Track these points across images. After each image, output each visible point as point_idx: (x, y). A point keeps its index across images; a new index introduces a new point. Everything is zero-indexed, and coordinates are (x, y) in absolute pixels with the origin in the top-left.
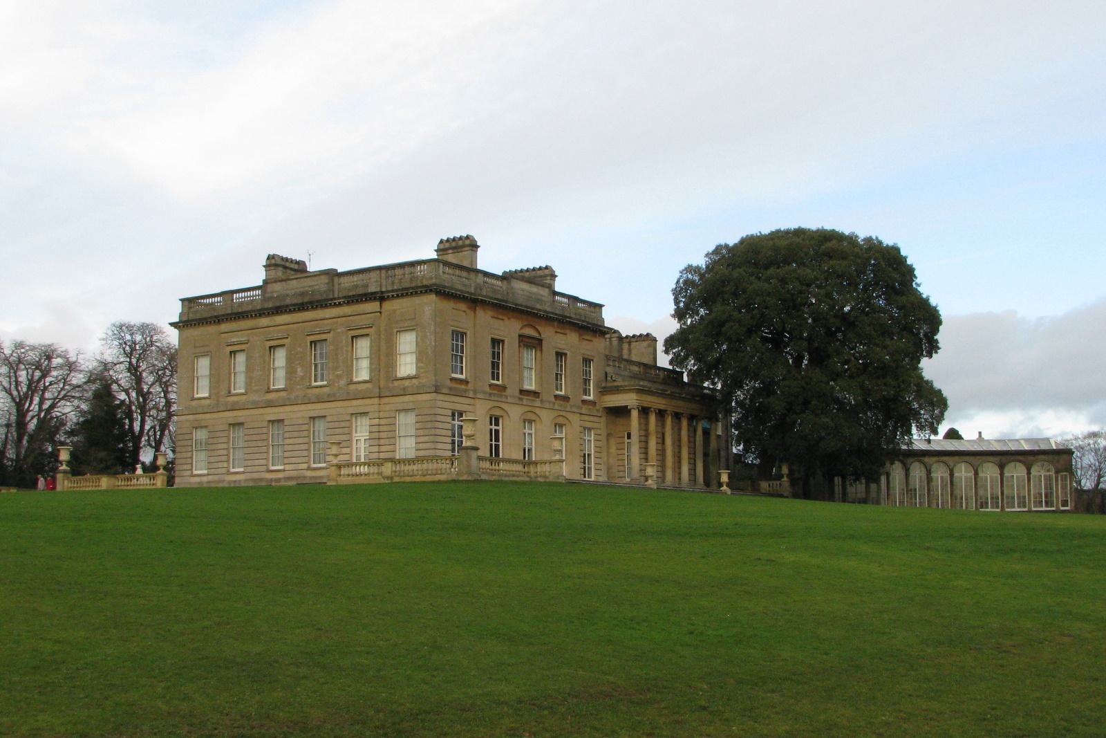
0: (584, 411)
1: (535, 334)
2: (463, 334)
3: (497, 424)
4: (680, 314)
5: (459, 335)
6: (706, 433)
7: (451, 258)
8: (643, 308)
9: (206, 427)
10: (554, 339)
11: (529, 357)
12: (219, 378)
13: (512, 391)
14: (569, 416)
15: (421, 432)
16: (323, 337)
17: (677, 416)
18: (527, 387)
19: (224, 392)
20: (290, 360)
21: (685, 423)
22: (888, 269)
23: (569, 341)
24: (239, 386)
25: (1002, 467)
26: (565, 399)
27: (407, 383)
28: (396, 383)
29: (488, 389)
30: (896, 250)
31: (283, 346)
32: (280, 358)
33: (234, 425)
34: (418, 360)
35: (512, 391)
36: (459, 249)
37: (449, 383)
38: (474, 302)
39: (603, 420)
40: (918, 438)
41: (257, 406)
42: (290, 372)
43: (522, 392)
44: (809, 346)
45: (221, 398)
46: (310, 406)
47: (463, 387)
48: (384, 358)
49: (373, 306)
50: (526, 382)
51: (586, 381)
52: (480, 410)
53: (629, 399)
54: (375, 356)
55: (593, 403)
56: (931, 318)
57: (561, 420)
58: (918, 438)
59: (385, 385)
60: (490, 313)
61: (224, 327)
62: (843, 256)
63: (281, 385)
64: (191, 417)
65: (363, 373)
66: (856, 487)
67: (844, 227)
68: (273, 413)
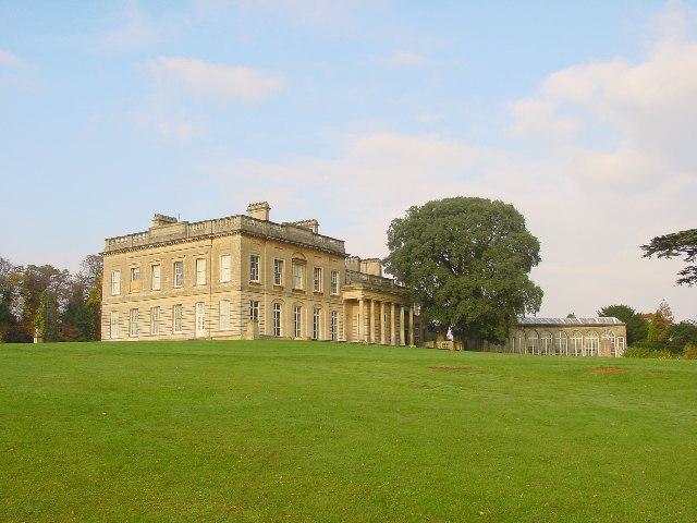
4: (391, 246)
5: (254, 259)
6: (407, 314)
8: (369, 243)
10: (314, 260)
11: (300, 271)
17: (388, 304)
18: (297, 288)
20: (163, 271)
21: (393, 308)
22: (506, 219)
23: (322, 261)
30: (510, 212)
38: (264, 239)
40: (529, 316)
44: (463, 274)
48: (213, 271)
53: (358, 294)
54: (209, 270)
58: (529, 316)
62: (480, 210)
63: (157, 287)
65: (201, 280)
67: (483, 196)
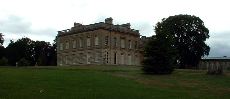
0: (135, 52)
1: (124, 36)
2: (108, 37)
3: (116, 54)
7: (108, 22)
9: (62, 56)
10: (128, 37)
11: (122, 41)
12: (64, 46)
13: (119, 48)
14: (132, 53)
15: (99, 56)
16: (82, 38)
18: (122, 47)
19: (65, 49)
22: (198, 21)
24: (74, 47)
25: (226, 63)
26: (131, 49)
27: (97, 46)
28: (95, 47)
29: (113, 48)
30: (199, 17)
31: (89, 38)
32: (75, 42)
33: (67, 55)
34: (99, 42)
35: (119, 48)
36: (109, 20)
37: (105, 46)
39: (139, 53)
40: (205, 57)
41: (70, 51)
42: (76, 45)
43: (121, 48)
45: (64, 51)
46: (79, 52)
47: (108, 47)
48: (93, 42)
49: (91, 32)
50: (122, 46)
51: (136, 46)
52: (112, 51)
55: (137, 50)
56: (207, 31)
57: (130, 54)
58: (205, 57)
59: (93, 47)
60: (114, 33)
61: (65, 37)
64: (60, 54)
66: (140, 66)
68: (73, 53)
